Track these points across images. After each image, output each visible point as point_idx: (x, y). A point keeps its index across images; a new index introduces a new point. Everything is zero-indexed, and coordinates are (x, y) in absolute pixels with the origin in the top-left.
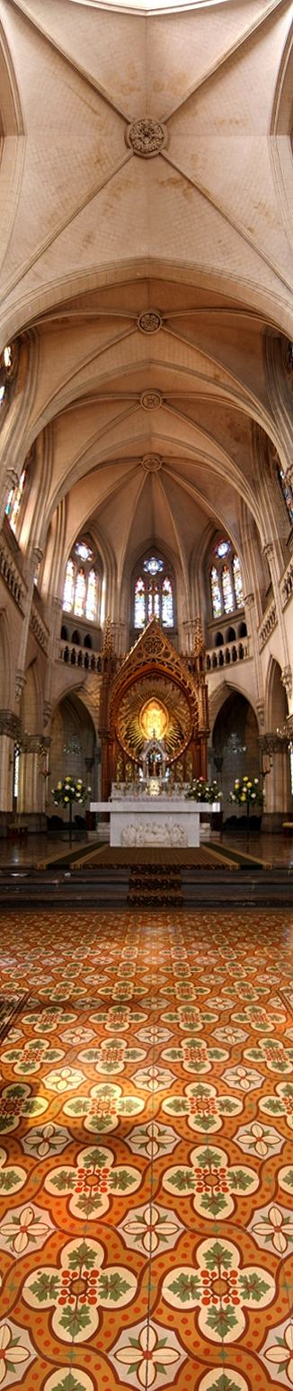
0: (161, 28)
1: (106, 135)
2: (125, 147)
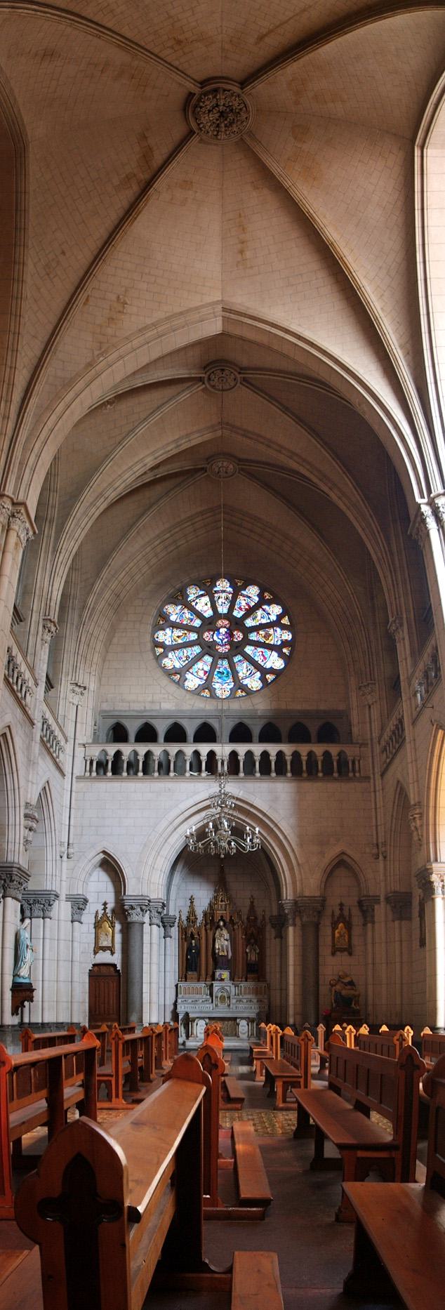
0: (394, 160)
1: (223, 49)
2: (11, 727)
